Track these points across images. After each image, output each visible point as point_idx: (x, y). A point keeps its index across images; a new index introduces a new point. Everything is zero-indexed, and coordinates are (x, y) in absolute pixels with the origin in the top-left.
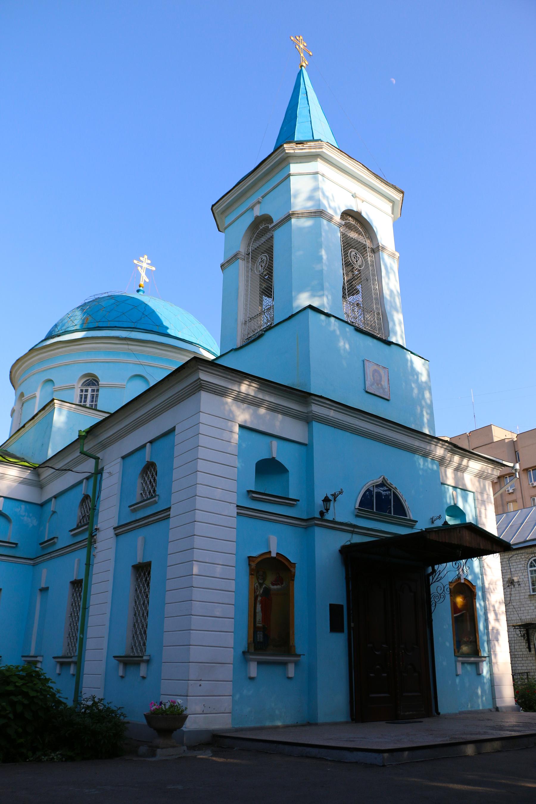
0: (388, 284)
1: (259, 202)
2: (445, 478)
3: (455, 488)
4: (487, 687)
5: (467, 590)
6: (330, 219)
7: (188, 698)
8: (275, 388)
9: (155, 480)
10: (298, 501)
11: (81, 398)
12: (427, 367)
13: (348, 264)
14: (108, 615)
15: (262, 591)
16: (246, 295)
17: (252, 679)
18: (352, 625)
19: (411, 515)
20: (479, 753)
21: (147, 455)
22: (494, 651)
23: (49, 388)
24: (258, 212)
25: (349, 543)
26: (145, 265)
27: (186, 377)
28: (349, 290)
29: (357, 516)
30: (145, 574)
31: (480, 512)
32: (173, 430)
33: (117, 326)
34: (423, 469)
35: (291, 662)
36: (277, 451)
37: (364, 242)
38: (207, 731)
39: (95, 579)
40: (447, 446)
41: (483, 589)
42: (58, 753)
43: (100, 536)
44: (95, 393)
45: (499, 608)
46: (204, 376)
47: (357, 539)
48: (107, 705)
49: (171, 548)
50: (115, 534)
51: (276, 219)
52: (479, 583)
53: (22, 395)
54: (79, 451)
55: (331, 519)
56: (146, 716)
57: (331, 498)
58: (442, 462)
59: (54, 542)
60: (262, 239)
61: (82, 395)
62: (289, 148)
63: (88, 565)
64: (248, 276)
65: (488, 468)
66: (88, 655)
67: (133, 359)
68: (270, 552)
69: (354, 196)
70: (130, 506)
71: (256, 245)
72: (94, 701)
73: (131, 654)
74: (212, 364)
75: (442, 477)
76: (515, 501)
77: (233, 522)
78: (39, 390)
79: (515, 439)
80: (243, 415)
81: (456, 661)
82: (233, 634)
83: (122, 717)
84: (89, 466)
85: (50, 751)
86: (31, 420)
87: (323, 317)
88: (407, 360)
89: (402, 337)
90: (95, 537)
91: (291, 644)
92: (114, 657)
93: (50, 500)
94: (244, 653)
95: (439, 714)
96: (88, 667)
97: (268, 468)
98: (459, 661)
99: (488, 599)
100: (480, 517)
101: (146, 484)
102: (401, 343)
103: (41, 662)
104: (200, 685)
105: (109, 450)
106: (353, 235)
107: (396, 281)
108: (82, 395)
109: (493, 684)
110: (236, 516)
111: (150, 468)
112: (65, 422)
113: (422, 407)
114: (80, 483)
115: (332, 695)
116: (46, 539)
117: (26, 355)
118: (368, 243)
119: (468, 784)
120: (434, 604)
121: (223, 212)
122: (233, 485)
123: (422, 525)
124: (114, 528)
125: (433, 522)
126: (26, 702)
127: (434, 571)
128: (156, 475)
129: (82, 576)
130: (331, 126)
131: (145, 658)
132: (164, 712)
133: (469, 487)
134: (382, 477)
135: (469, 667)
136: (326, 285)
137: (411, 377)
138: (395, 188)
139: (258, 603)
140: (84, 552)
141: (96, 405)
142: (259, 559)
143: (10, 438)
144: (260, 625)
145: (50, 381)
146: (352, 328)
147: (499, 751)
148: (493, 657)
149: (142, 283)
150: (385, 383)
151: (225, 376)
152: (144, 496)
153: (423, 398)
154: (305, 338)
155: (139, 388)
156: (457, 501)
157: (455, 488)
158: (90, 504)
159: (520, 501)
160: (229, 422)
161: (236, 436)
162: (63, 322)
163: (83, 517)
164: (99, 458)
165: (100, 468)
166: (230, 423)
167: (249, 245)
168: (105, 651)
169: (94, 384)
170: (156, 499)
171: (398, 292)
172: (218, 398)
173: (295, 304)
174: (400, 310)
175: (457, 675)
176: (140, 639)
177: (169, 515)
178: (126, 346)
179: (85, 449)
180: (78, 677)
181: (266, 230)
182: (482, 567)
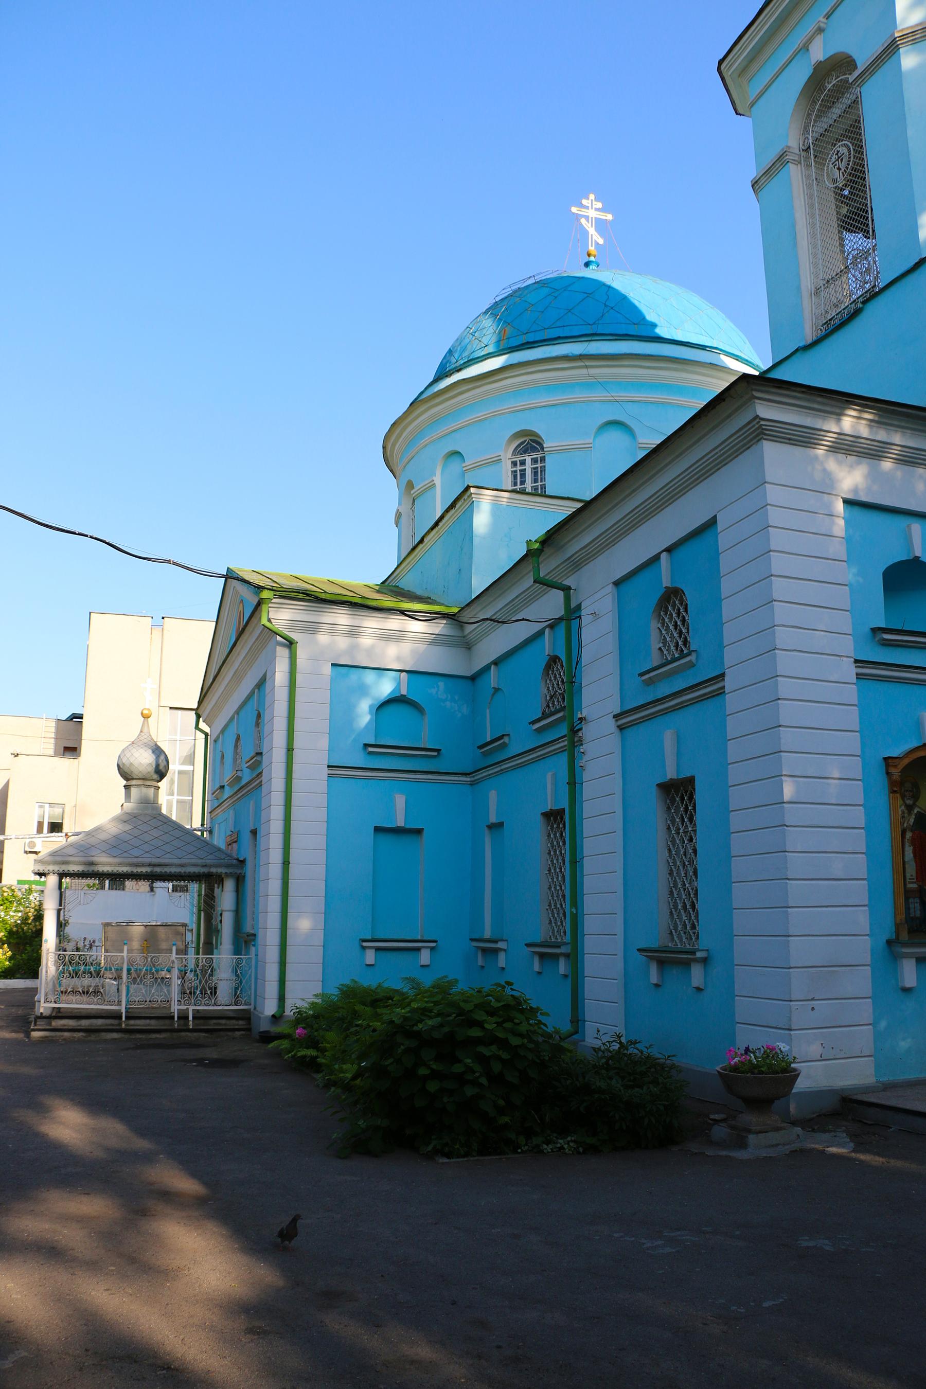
1: (820, 30)
7: (792, 1033)
8: (908, 416)
9: (683, 621)
11: (515, 477)
15: (912, 820)
16: (813, 235)
17: (907, 990)
21: (665, 575)
23: (456, 466)
24: (819, 52)
26: (592, 214)
27: (729, 416)
30: (682, 799)
33: (561, 335)
38: (832, 1092)
39: (588, 809)
42: (569, 1139)
43: (588, 732)
44: (539, 465)
46: (766, 411)
48: (644, 1050)
49: (733, 751)
50: (618, 727)
51: (862, 62)
53: (410, 485)
59: (504, 743)
60: (834, 110)
61: (516, 472)
63: (573, 784)
64: (811, 196)
66: (589, 944)
67: (599, 394)
70: (641, 675)
72: (621, 1043)
77: (851, 693)
80: (851, 478)
82: (866, 908)
84: (551, 605)
85: (555, 1135)
86: (432, 528)
90: (580, 734)
93: (487, 668)
94: (889, 943)
96: (591, 964)
103: (505, 950)
104: (813, 1009)
105: (587, 570)
108: (516, 472)
110: (855, 681)
111: (672, 598)
112: (498, 528)
114: (540, 633)
116: (488, 739)
122: (844, 622)
124: (615, 717)
126: (505, 1056)
128: (686, 610)
129: (564, 804)
131: (699, 955)
132: (753, 1068)
139: (907, 844)
140: (563, 759)
141: (543, 487)
142: (906, 761)
144: (915, 886)
145: (456, 453)
149: (592, 249)
152: (665, 652)
158: (562, 674)
161: (841, 522)
163: (551, 697)
164: (569, 588)
167: (806, 130)
169: (534, 449)
170: (693, 658)
172: (797, 451)
176: (684, 918)
177: (724, 687)
178: (584, 371)
180: (575, 979)
181: (843, 88)
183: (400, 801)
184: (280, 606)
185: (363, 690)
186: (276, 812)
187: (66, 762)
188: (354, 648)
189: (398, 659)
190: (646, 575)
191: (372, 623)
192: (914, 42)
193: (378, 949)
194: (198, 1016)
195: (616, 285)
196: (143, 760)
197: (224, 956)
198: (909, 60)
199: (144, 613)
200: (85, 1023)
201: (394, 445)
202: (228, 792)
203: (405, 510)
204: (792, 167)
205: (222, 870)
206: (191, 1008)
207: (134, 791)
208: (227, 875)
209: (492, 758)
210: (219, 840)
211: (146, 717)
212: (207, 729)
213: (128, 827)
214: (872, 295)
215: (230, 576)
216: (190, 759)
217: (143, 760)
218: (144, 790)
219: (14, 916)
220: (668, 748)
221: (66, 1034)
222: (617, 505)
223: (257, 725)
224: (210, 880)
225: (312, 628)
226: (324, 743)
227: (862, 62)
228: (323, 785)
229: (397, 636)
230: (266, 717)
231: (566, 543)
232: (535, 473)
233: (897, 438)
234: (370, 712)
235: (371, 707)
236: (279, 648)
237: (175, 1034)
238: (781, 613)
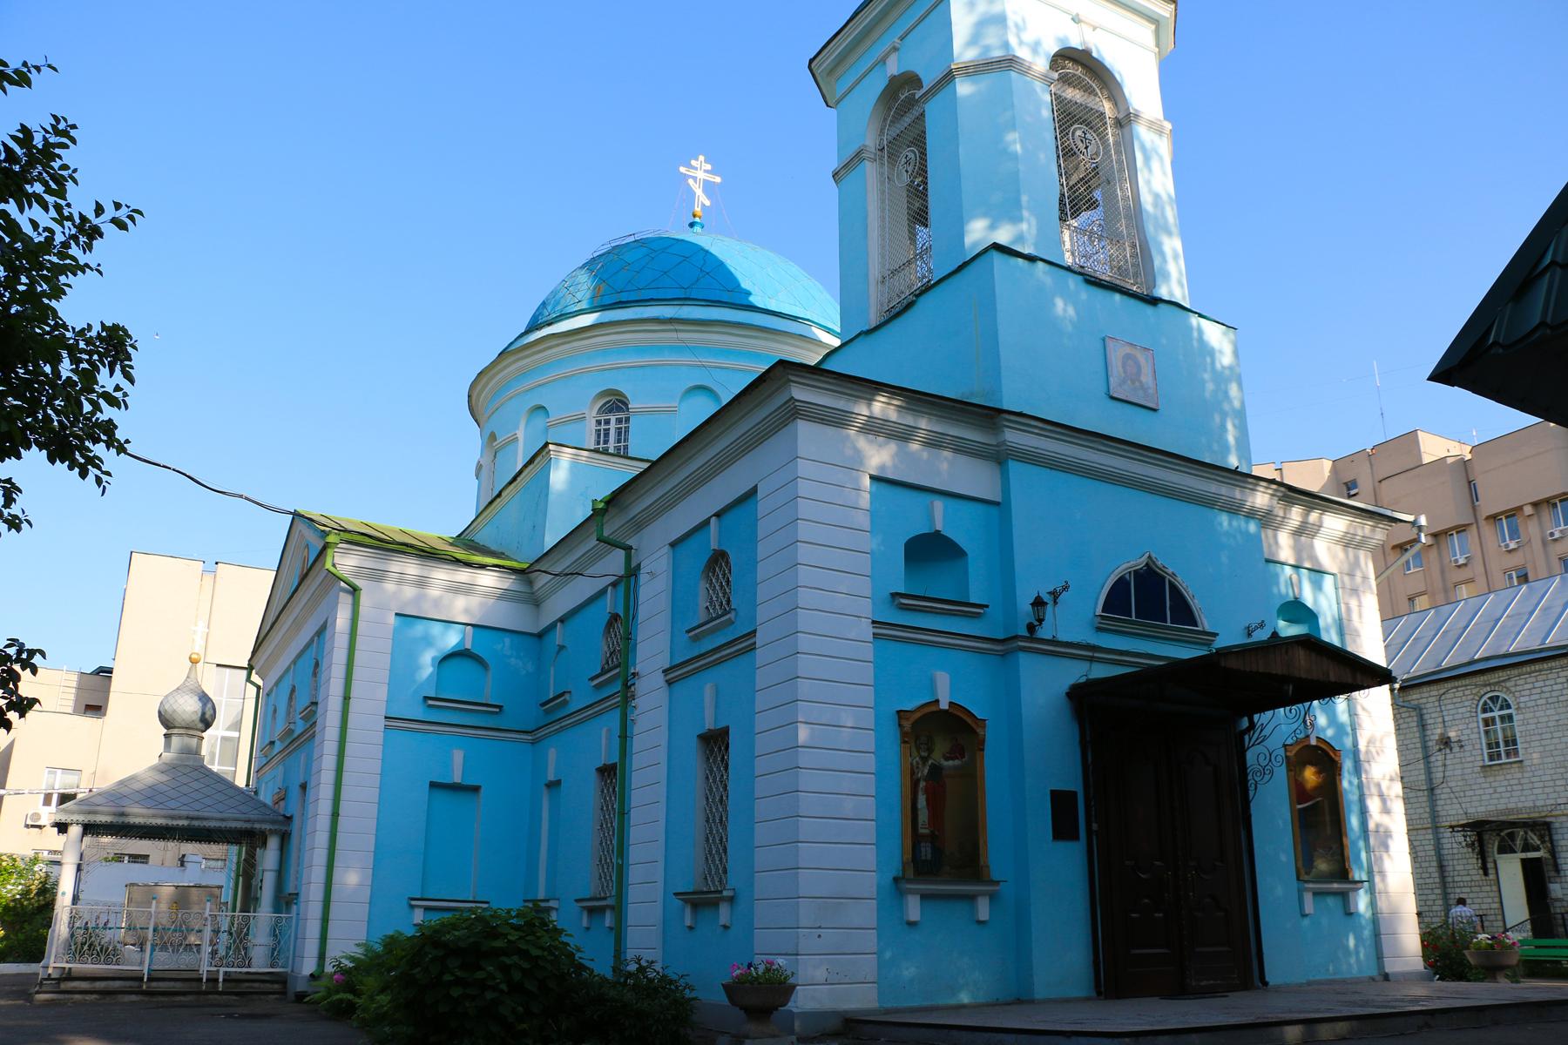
0: (1148, 182)
1: (895, 49)
3: (1296, 567)
4: (1367, 933)
5: (1325, 758)
9: (728, 582)
13: (1067, 153)
14: (662, 823)
16: (882, 228)
17: (912, 924)
18: (1095, 826)
19: (1206, 624)
21: (713, 538)
22: (1382, 873)
23: (540, 421)
24: (893, 67)
25: (1083, 680)
26: (701, 175)
28: (1073, 203)
29: (1099, 629)
31: (1349, 609)
32: (753, 492)
35: (983, 894)
36: (942, 518)
38: (835, 1013)
39: (637, 761)
43: (641, 687)
45: (1389, 788)
47: (1100, 672)
49: (761, 701)
51: (928, 82)
52: (1348, 742)
53: (493, 437)
54: (594, 537)
55: (1049, 637)
56: (727, 988)
57: (1046, 598)
58: (1267, 520)
63: (624, 737)
64: (883, 192)
65: (1365, 528)
66: (634, 893)
68: (937, 701)
69: (1076, 20)
71: (895, 131)
74: (816, 370)
75: (1270, 546)
76: (1471, 580)
77: (867, 651)
79: (1469, 457)
80: (879, 456)
81: (1300, 892)
84: (614, 563)
86: (510, 483)
88: (1190, 328)
89: (1180, 283)
93: (552, 626)
94: (896, 880)
95: (1265, 984)
96: (634, 914)
97: (929, 550)
98: (1308, 890)
102: (1178, 298)
106: (1072, 94)
107: (1165, 173)
109: (1378, 931)
110: (870, 638)
111: (718, 559)
112: (573, 482)
113: (1224, 415)
114: (603, 592)
115: (1061, 952)
118: (1107, 107)
122: (865, 587)
123: (1230, 636)
125: (1249, 635)
126: (526, 965)
127: (1252, 726)
129: (615, 759)
131: (725, 893)
140: (617, 714)
141: (626, 447)
142: (918, 715)
148: (1377, 879)
149: (698, 209)
150: (1147, 378)
154: (987, 304)
155: (703, 409)
157: (1296, 567)
158: (621, 628)
159: (1482, 581)
160: (848, 481)
161: (865, 500)
165: (633, 564)
167: (882, 131)
168: (660, 885)
169: (619, 409)
170: (732, 615)
172: (830, 431)
173: (969, 239)
174: (1174, 229)
175: (1304, 916)
178: (674, 335)
180: (618, 931)
181: (911, 102)
182: (1352, 713)
183: (458, 757)
184: (346, 552)
185: (427, 641)
186: (328, 762)
187: (89, 722)
188: (419, 599)
189: (467, 611)
190: (697, 537)
191: (441, 575)
192: (968, 75)
193: (427, 909)
194: (228, 979)
195: (713, 250)
196: (188, 707)
197: (264, 914)
198: (963, 88)
199: (195, 556)
200: (99, 985)
202: (278, 747)
203: (486, 462)
205: (266, 827)
206: (222, 970)
207: (175, 740)
208: (272, 832)
209: (554, 713)
210: (266, 797)
211: (194, 662)
212: (260, 682)
213: (164, 778)
214: (927, 288)
215: (296, 515)
216: (237, 726)
217: (188, 707)
218: (186, 739)
219: (11, 889)
220: (707, 702)
221: (77, 997)
223: (315, 674)
224: (248, 838)
225: (378, 576)
227: (928, 82)
228: (378, 737)
229: (466, 589)
230: (324, 666)
233: (923, 423)
235: (434, 659)
236: (342, 594)
237: (202, 997)
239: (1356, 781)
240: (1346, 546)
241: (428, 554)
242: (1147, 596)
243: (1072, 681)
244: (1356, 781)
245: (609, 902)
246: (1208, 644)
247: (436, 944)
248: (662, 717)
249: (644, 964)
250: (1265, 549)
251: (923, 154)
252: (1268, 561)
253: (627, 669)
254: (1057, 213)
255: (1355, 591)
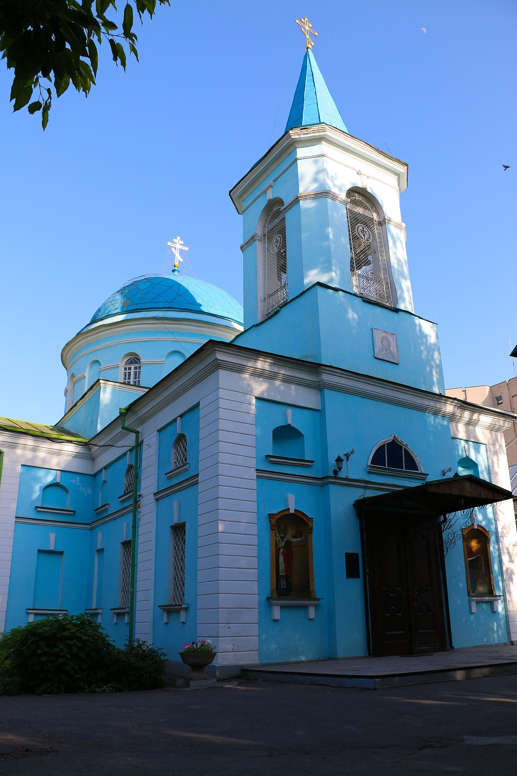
1: (271, 186)
2: (456, 432)
3: (467, 441)
5: (482, 535)
6: (334, 197)
9: (186, 450)
10: (314, 462)
11: (126, 376)
12: (435, 328)
13: (354, 238)
15: (283, 544)
16: (264, 274)
17: (276, 621)
18: (367, 571)
19: (422, 469)
20: (468, 678)
21: (178, 428)
22: (509, 591)
23: (96, 368)
24: (270, 195)
25: (361, 498)
26: (178, 246)
28: (358, 262)
29: (369, 473)
31: (492, 462)
32: (197, 405)
34: (433, 425)
35: (312, 605)
36: (291, 417)
37: (371, 217)
38: (237, 666)
39: (141, 539)
40: (456, 403)
41: (497, 533)
43: (143, 502)
44: (138, 370)
45: (513, 550)
47: (370, 494)
49: (201, 509)
51: (287, 202)
52: (493, 527)
53: (73, 376)
54: (121, 427)
55: (345, 477)
57: (343, 457)
58: (452, 418)
61: (126, 373)
62: (295, 134)
63: (135, 527)
64: (265, 256)
66: (138, 606)
67: (170, 337)
68: (289, 509)
70: (166, 474)
72: (139, 643)
73: (174, 604)
74: (230, 346)
75: (454, 431)
77: (254, 484)
78: (87, 370)
80: (260, 388)
81: (470, 602)
83: (162, 657)
84: (130, 440)
86: (81, 399)
87: (331, 291)
88: (415, 324)
89: (410, 302)
90: (139, 503)
91: (311, 590)
92: (159, 606)
93: (100, 471)
94: (268, 599)
95: (453, 648)
96: (139, 616)
97: (285, 434)
98: (473, 600)
99: (502, 542)
100: (493, 467)
101: (179, 453)
102: (409, 309)
103: (101, 614)
104: (229, 628)
106: (360, 210)
107: (403, 249)
108: (126, 373)
111: (181, 438)
112: (111, 398)
113: (431, 367)
114: (125, 454)
115: (350, 632)
117: (74, 339)
118: (375, 216)
119: (440, 700)
120: (446, 550)
121: (240, 197)
122: (252, 452)
123: (434, 476)
125: (444, 475)
126: (80, 645)
127: (445, 520)
129: (130, 538)
130: (337, 106)
132: (195, 651)
133: (482, 439)
134: (393, 436)
135: (484, 606)
136: (334, 261)
137: (420, 341)
138: (399, 161)
139: (280, 555)
140: (131, 516)
141: (139, 381)
142: (279, 516)
143: (65, 416)
144: (284, 574)
145: (97, 361)
146: (360, 299)
147: (488, 676)
148: (507, 595)
149: (177, 263)
150: (393, 348)
151: (239, 354)
153: (433, 359)
155: (178, 361)
156: (469, 453)
157: (467, 441)
158: (134, 472)
160: (246, 397)
161: (254, 407)
162: (106, 307)
164: (139, 432)
165: (140, 440)
166: (248, 397)
168: (152, 602)
169: (136, 362)
170: (187, 466)
171: (405, 260)
174: (408, 277)
177: (198, 480)
178: (163, 326)
179: (126, 425)
180: (131, 625)
181: (279, 213)
182: (495, 513)
183: (53, 537)
185: (37, 480)
188: (35, 458)
189: (58, 464)
191: (47, 445)
193: (36, 614)
201: (67, 355)
204: (257, 242)
209: (101, 516)
214: (285, 304)
220: (175, 509)
222: (159, 394)
225: (13, 446)
226: (14, 505)
227: (287, 202)
229: (59, 453)
231: (138, 411)
232: (135, 373)
233: (283, 372)
234: (40, 491)
235: (40, 487)
238: (222, 447)
239: (497, 547)
240: (491, 430)
241: (39, 436)
242: (393, 455)
243: (356, 498)
244: (497, 547)
245: (127, 610)
246: (423, 479)
247: (34, 634)
248: (153, 517)
249: (141, 642)
250: (452, 433)
251: (284, 238)
252: (453, 438)
253: (137, 493)
254: (349, 267)
255: (496, 453)
